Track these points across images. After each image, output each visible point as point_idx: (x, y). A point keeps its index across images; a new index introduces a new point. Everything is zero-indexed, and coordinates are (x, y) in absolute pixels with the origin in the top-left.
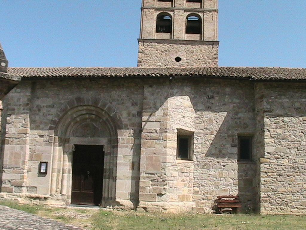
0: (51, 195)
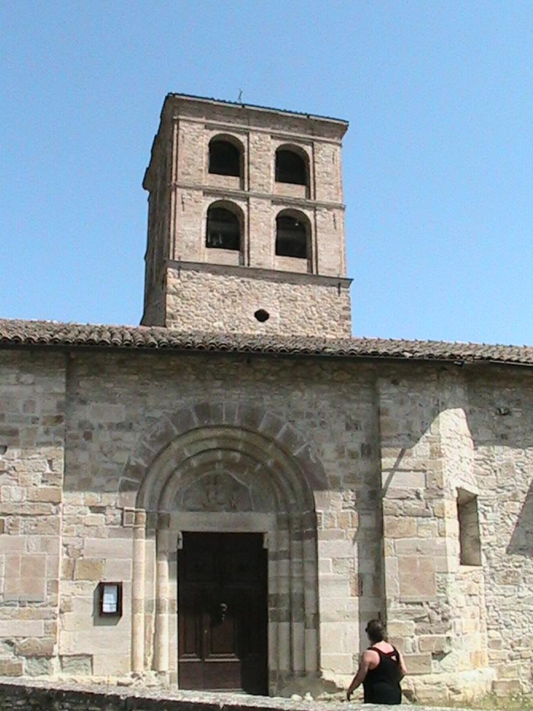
0: (133, 676)
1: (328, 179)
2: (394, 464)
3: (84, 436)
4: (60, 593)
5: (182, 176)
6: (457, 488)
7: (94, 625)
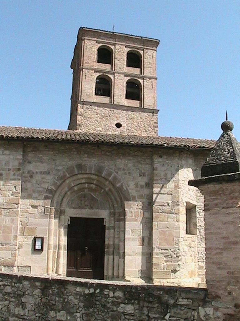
1: (150, 66)
2: (158, 191)
3: (30, 177)
4: (18, 241)
5: (85, 64)
6: (186, 202)
7: (32, 254)
